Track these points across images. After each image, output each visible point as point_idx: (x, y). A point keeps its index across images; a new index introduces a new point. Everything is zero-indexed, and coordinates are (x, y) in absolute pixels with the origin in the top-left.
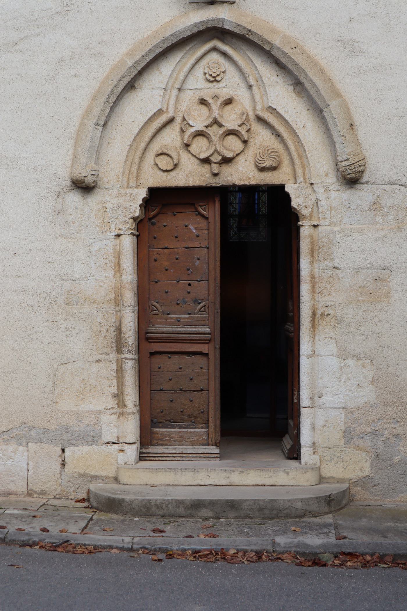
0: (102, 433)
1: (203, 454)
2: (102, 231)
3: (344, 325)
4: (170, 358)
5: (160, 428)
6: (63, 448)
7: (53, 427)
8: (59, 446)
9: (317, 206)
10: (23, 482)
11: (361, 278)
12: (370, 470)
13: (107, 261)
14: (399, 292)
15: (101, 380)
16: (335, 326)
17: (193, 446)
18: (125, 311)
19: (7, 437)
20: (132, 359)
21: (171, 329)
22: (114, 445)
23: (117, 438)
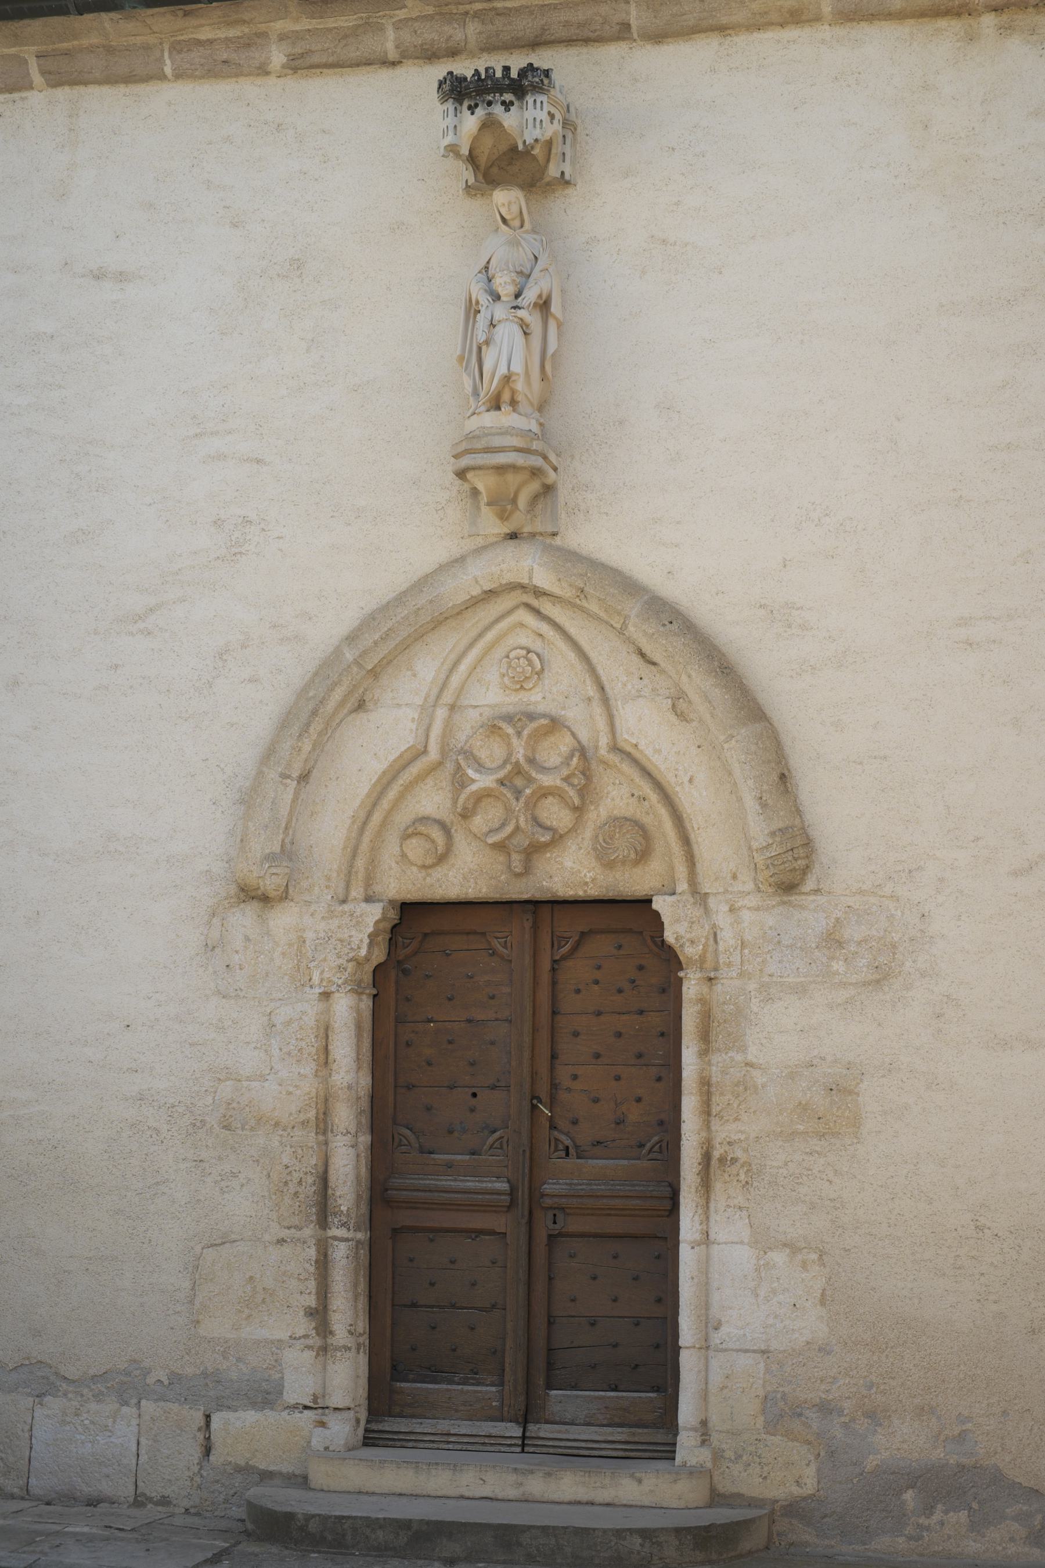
0: (283, 1387)
1: (489, 1438)
2: (296, 985)
3: (765, 1182)
4: (432, 1240)
5: (408, 1381)
6: (207, 1413)
7: (189, 1371)
8: (199, 1409)
9: (716, 941)
10: (128, 1478)
11: (801, 1085)
12: (815, 1484)
13: (303, 1044)
14: (876, 1115)
15: (285, 1279)
16: (747, 1183)
17: (472, 1420)
18: (335, 1144)
19: (99, 1386)
20: (347, 1240)
21: (434, 1182)
22: (306, 1412)
23: (312, 1397)
